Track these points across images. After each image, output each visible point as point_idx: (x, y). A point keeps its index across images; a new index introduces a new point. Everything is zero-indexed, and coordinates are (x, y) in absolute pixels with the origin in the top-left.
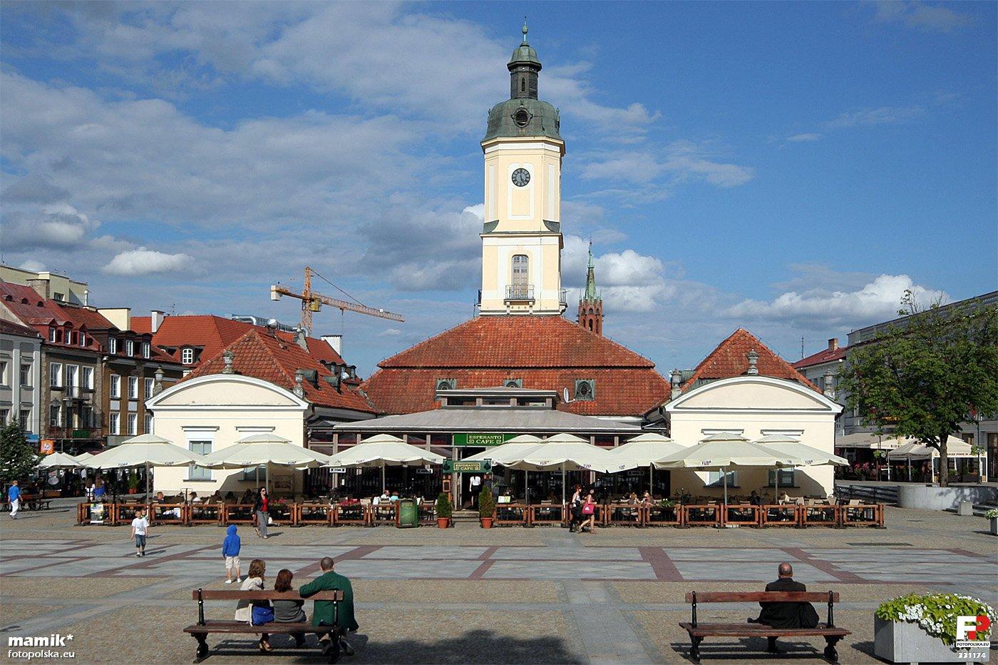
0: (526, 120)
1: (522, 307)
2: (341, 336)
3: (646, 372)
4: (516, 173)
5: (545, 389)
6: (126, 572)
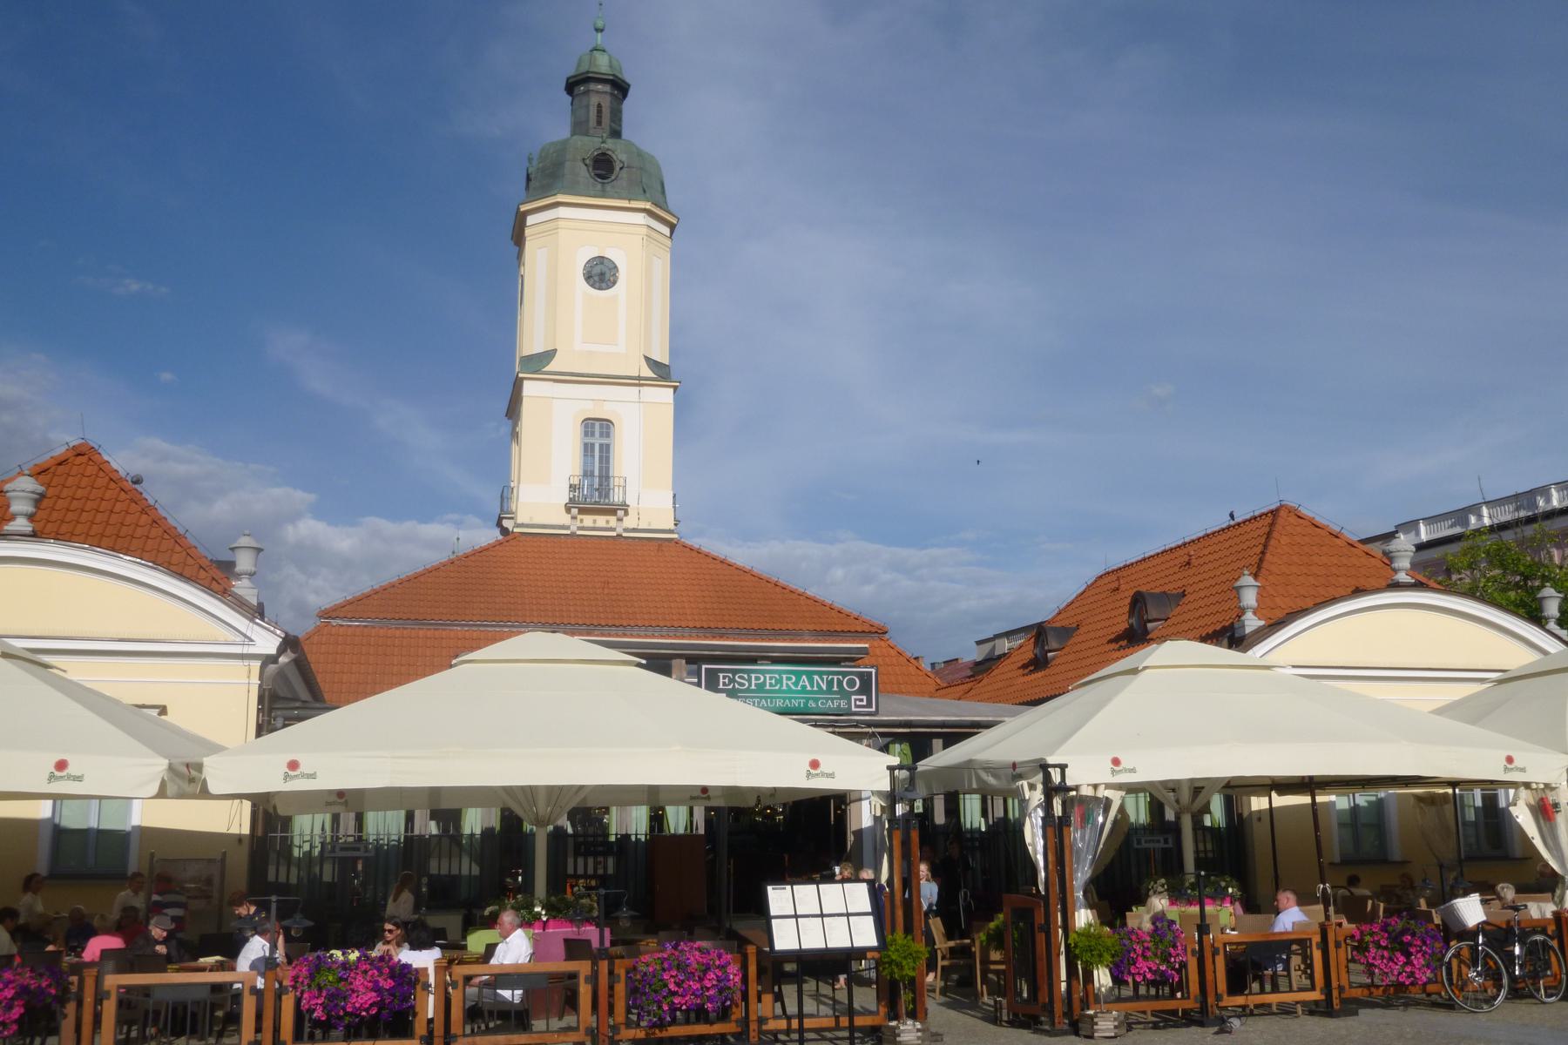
1: (601, 521)
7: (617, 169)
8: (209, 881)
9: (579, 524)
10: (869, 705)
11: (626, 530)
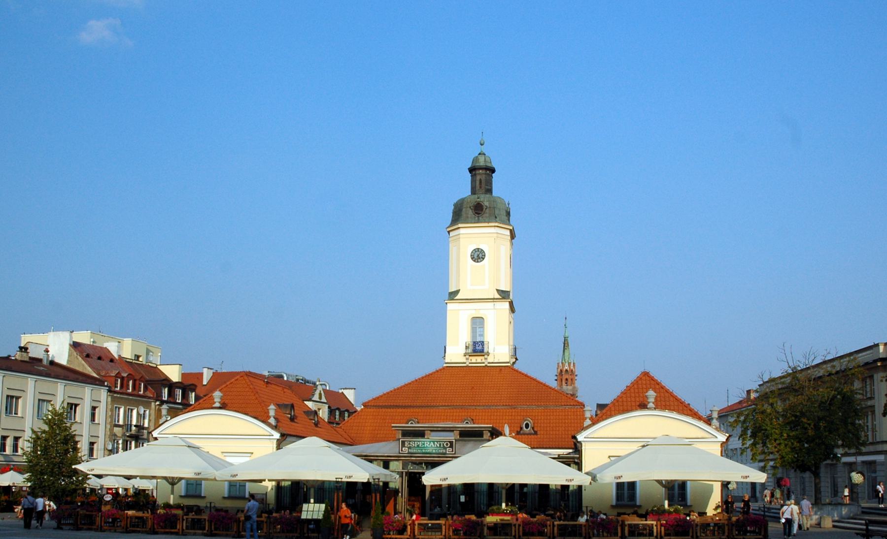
0: (482, 210)
2: (355, 389)
4: (474, 252)
5: (484, 424)
7: (484, 209)
8: (263, 500)
9: (470, 361)
10: (453, 451)
11: (489, 363)
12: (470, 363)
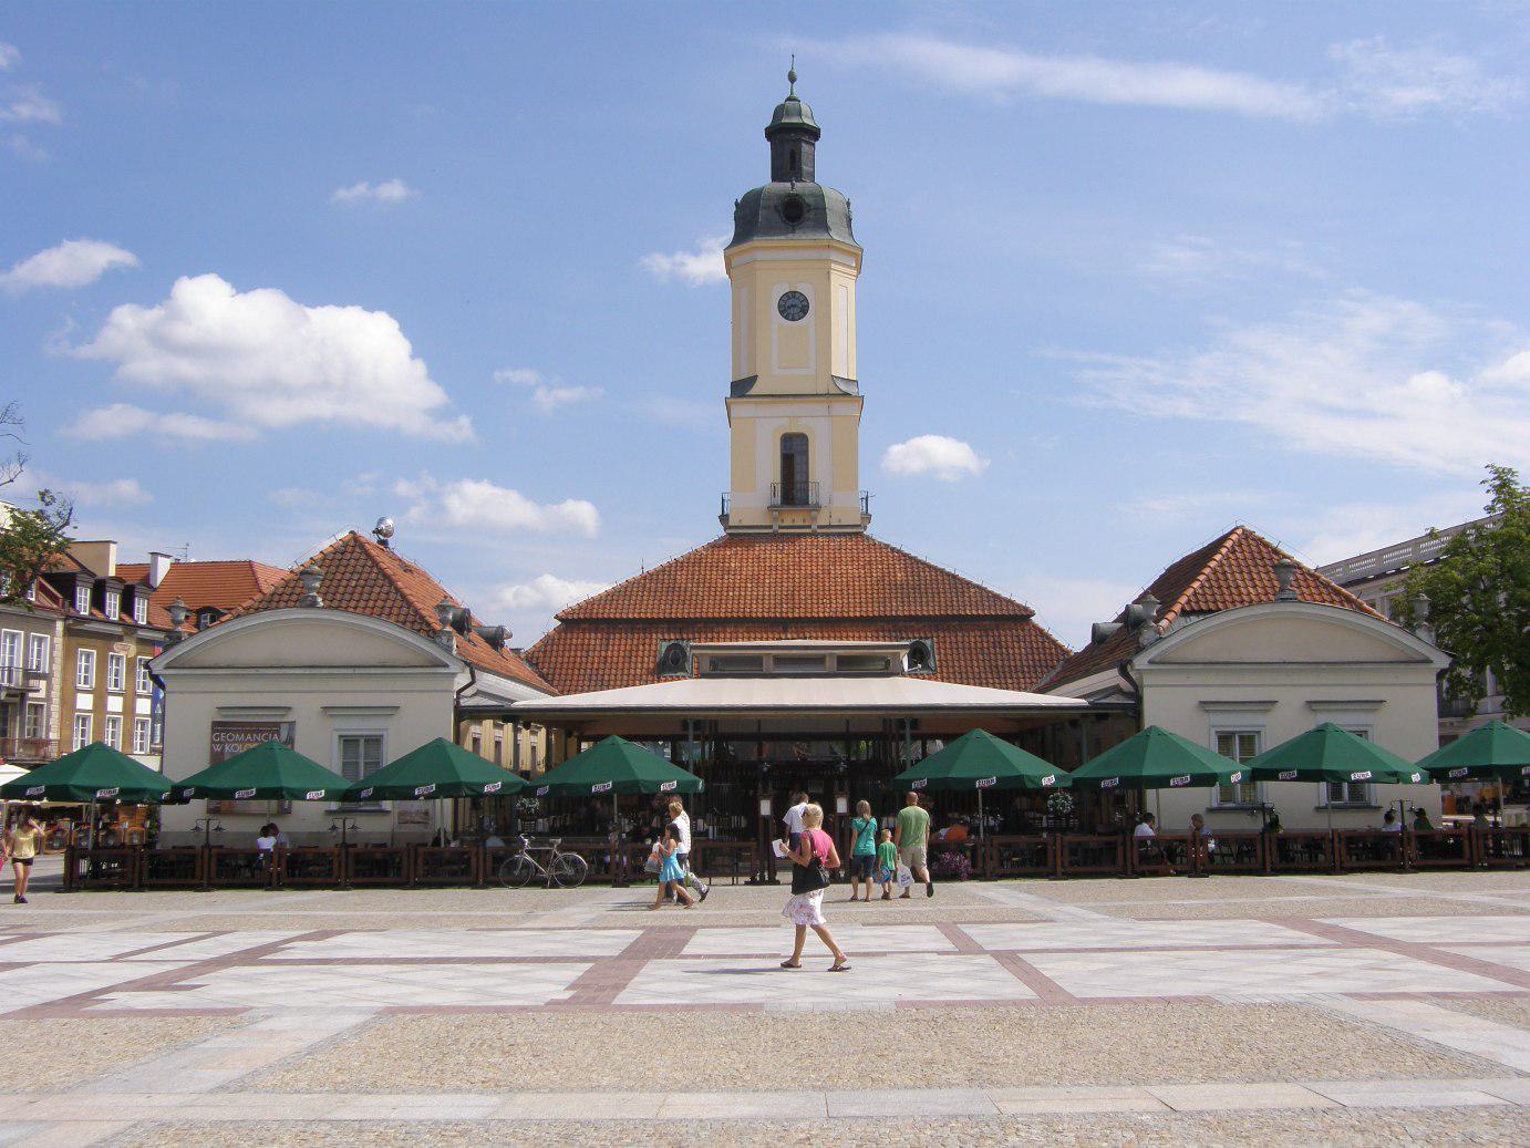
3: (1006, 635)
6: (123, 1000)
12: (780, 527)
